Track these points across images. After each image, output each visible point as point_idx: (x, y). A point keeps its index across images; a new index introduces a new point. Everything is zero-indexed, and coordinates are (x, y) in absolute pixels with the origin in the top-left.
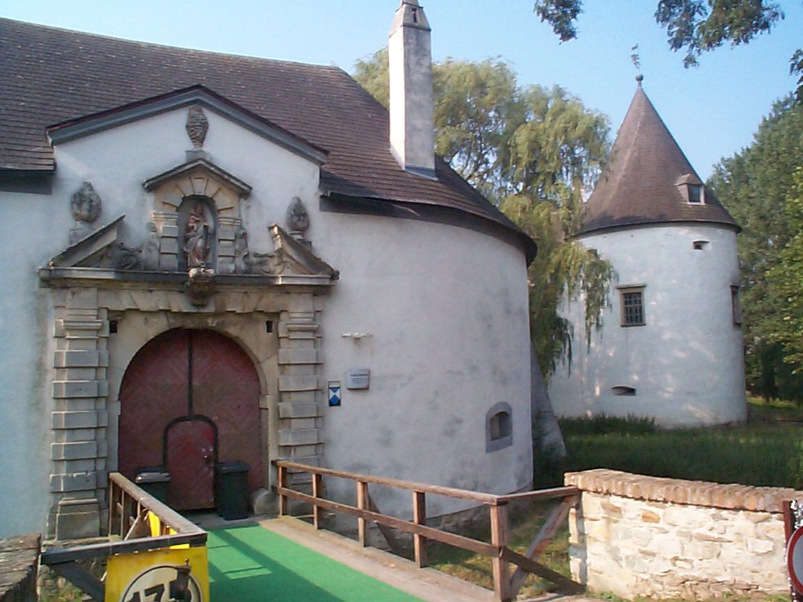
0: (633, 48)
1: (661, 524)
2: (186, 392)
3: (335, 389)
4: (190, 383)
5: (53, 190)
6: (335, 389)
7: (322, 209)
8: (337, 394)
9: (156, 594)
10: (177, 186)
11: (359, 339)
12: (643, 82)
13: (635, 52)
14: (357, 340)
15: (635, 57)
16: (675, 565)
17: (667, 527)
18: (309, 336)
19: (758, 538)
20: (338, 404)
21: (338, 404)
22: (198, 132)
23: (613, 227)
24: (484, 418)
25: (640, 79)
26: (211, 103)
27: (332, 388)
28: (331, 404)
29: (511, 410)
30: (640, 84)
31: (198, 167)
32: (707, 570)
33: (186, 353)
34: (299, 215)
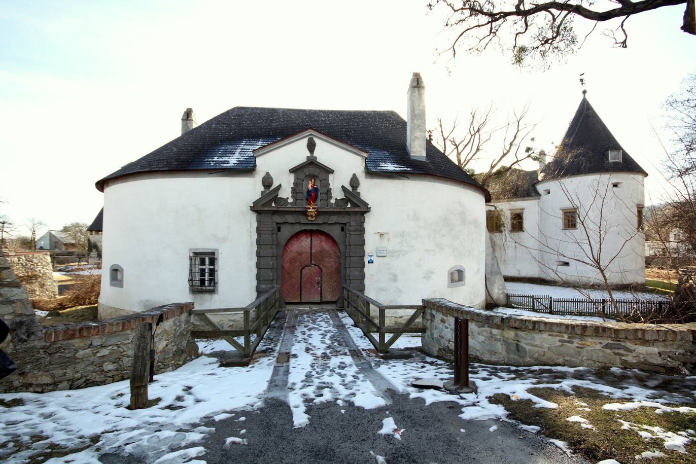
0: (581, 75)
1: (446, 324)
2: (309, 255)
3: (371, 256)
4: (311, 251)
5: (256, 175)
6: (371, 256)
7: (366, 177)
8: (372, 258)
9: (386, 341)
10: (303, 171)
11: (382, 234)
12: (586, 94)
13: (582, 77)
14: (381, 235)
15: (582, 80)
16: (449, 344)
17: (448, 326)
18: (359, 233)
19: (479, 334)
20: (373, 262)
21: (373, 262)
22: (311, 146)
23: (414, 174)
24: (447, 273)
25: (584, 92)
26: (316, 135)
27: (370, 256)
28: (369, 262)
29: (465, 270)
30: (584, 96)
31: (312, 162)
32: (477, 352)
33: (309, 239)
34: (355, 182)
